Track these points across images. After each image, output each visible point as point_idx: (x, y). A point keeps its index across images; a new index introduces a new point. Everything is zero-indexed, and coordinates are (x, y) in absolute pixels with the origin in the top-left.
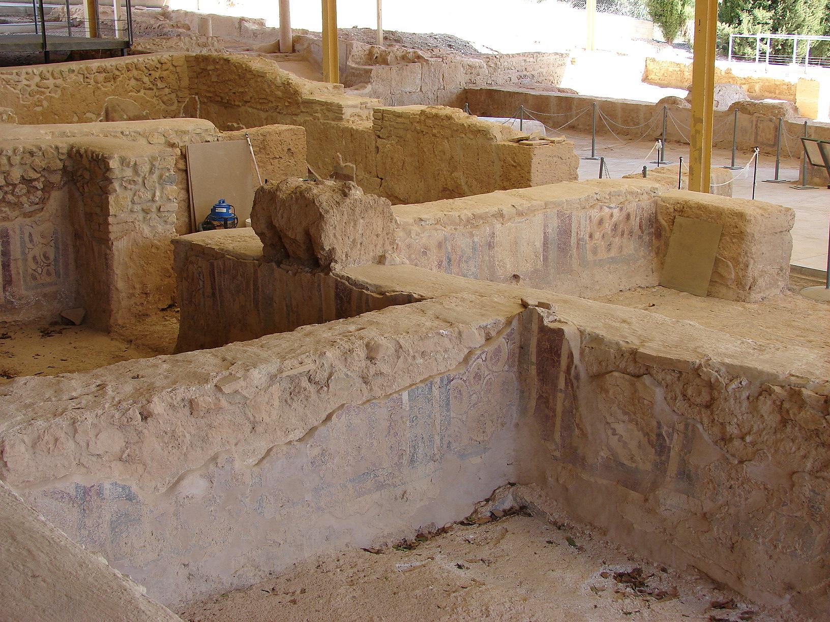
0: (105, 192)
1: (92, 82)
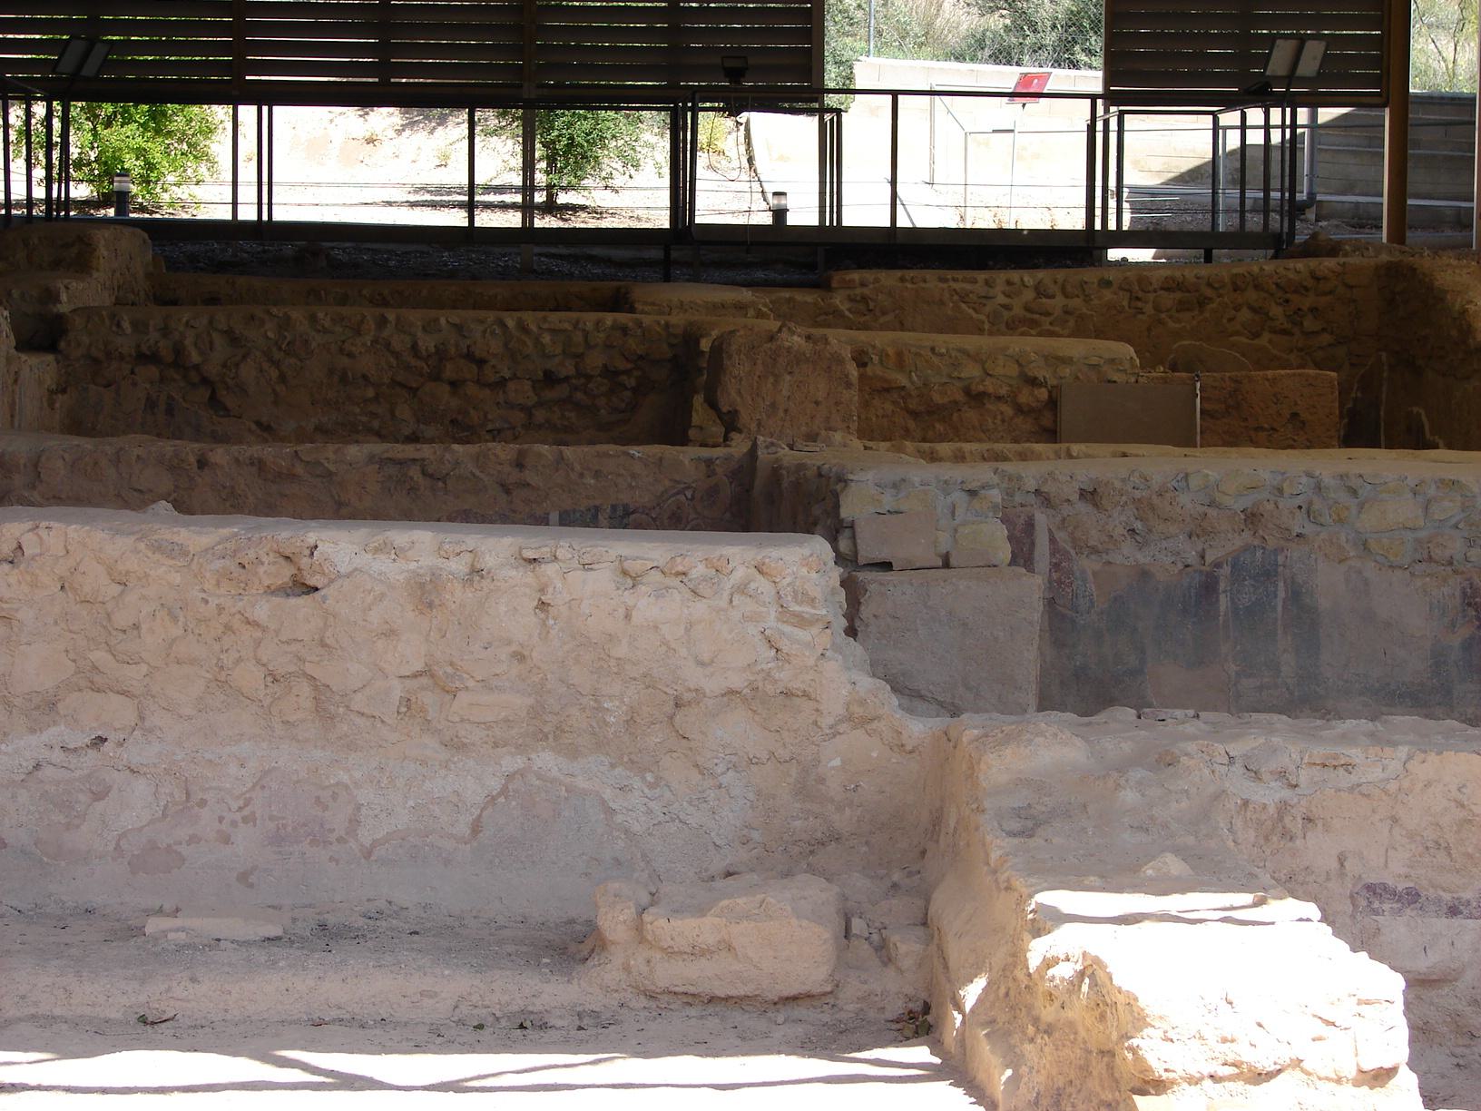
1: (1149, 309)
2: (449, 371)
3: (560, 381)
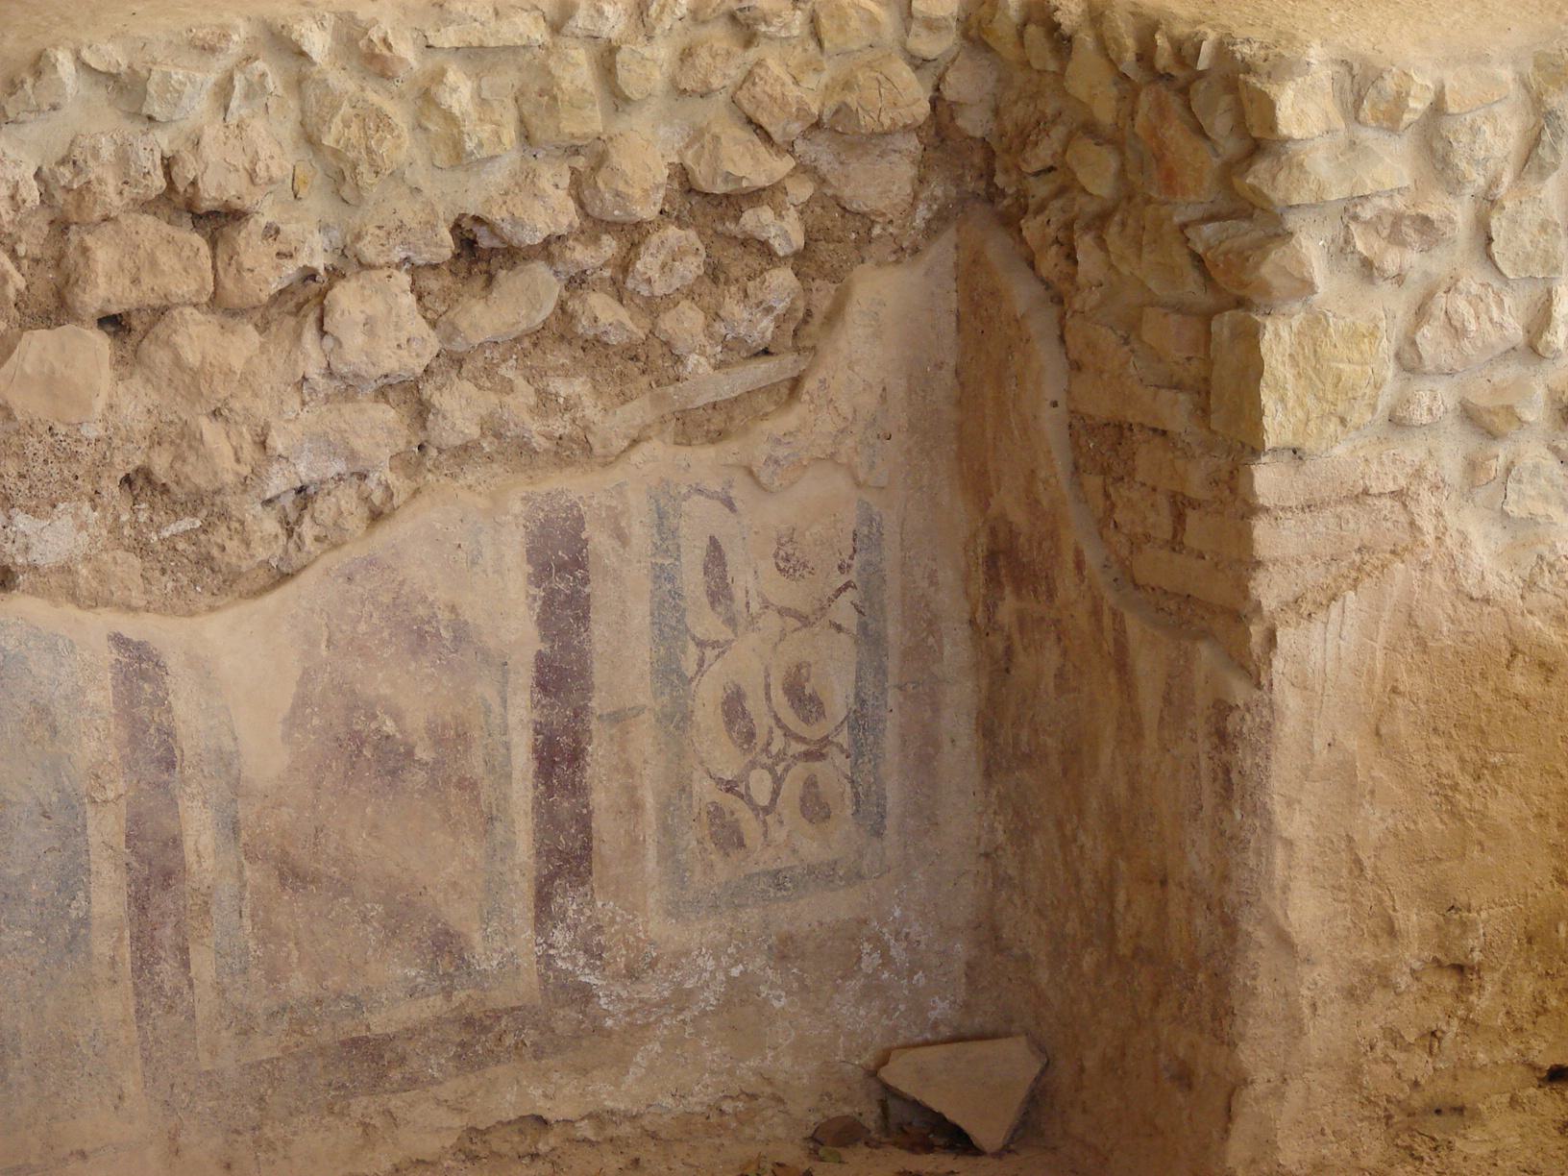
0: (1227, 295)
2: (105, 284)
3: (513, 255)
